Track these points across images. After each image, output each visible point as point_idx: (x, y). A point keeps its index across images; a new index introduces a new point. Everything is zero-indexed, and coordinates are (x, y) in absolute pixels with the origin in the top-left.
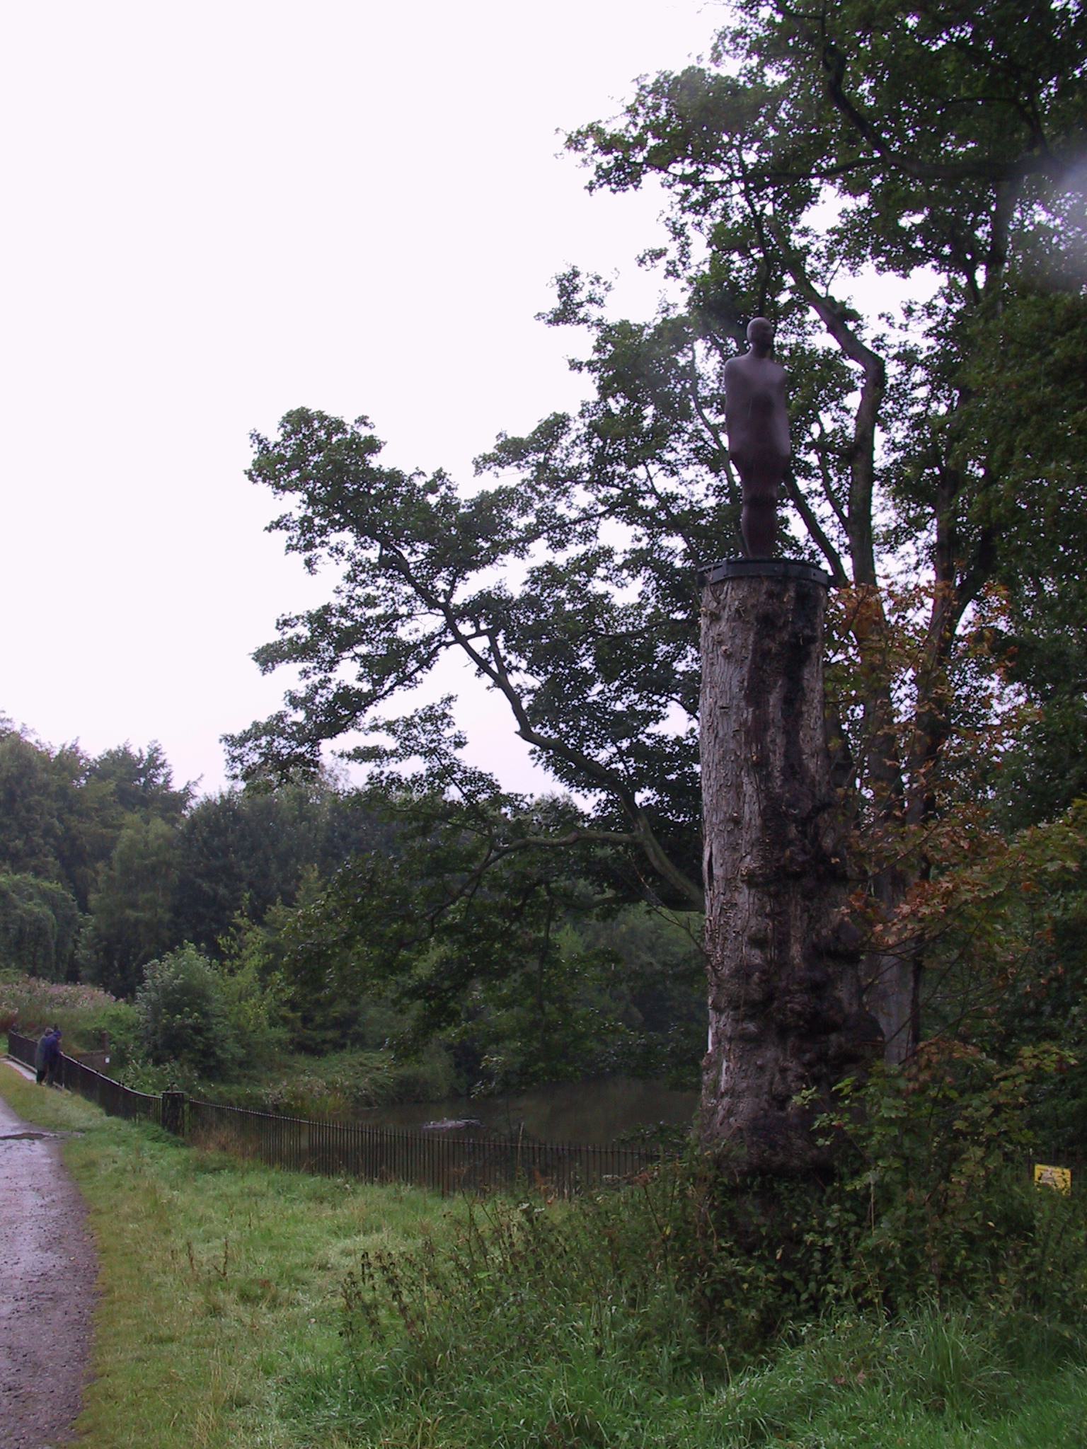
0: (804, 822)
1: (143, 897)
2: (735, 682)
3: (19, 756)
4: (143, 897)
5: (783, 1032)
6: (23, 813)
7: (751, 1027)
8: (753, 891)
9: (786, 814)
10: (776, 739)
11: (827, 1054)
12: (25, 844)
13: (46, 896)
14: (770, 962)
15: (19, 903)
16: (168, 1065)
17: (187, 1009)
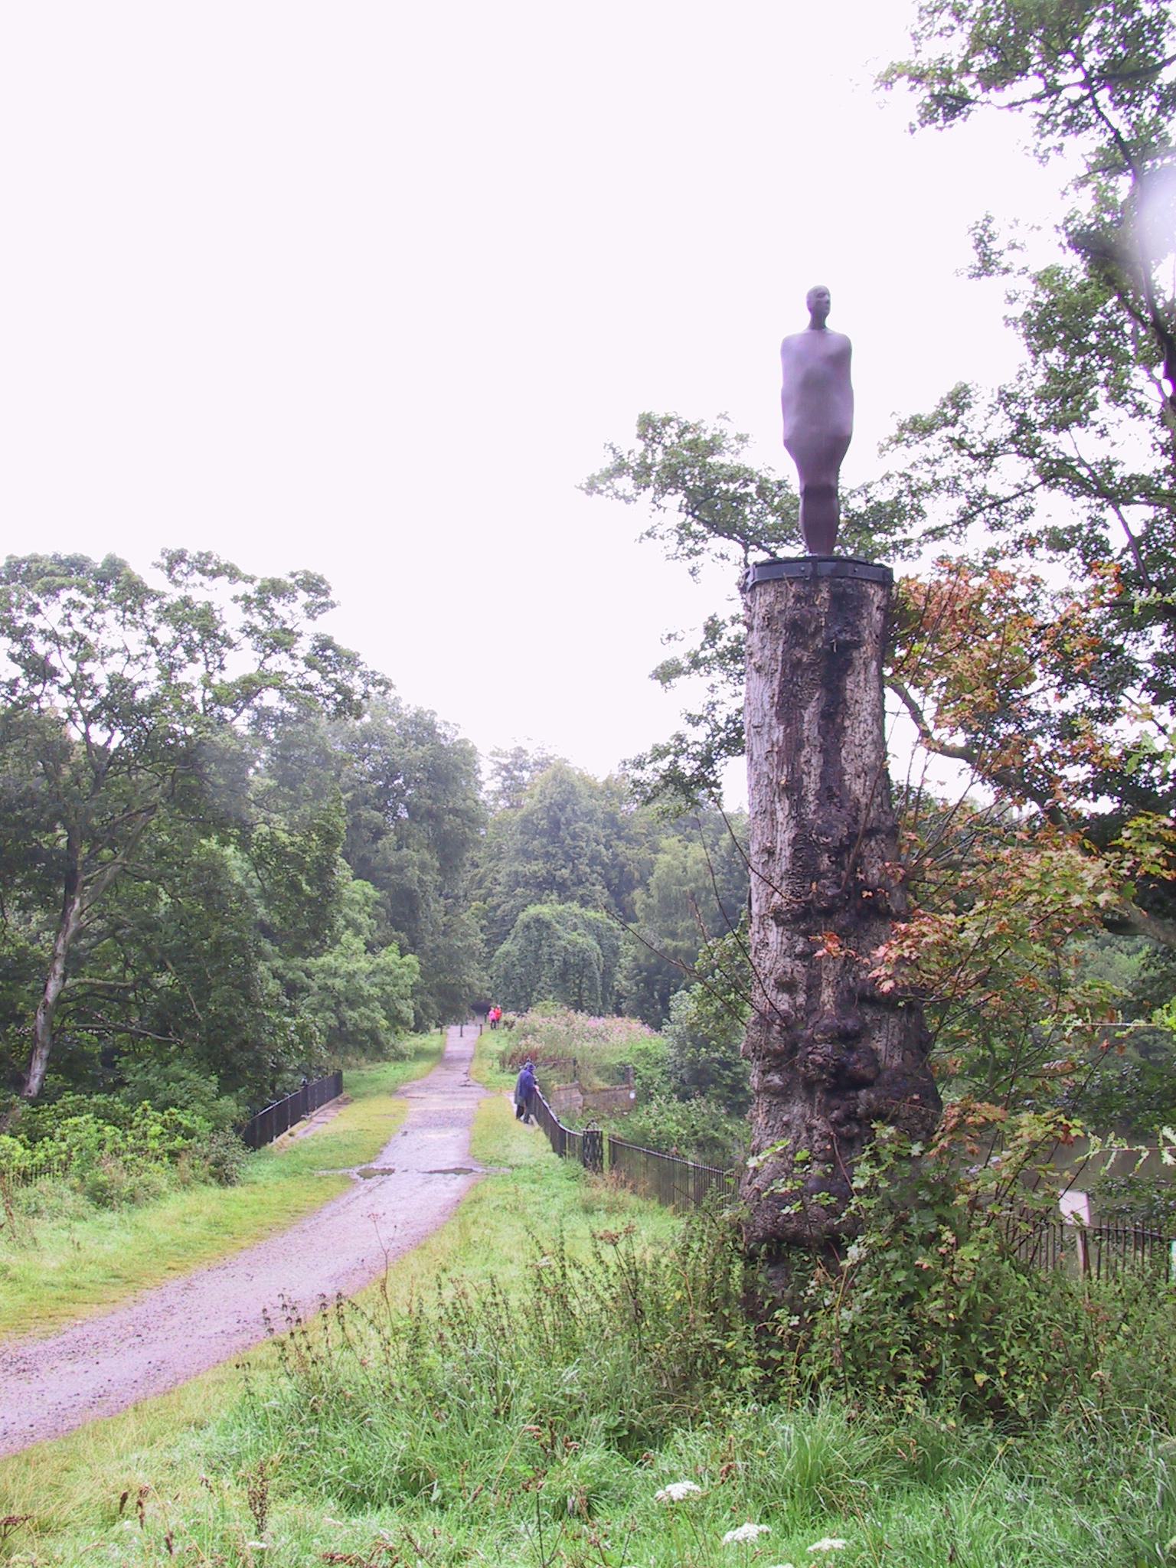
0: (839, 852)
1: (682, 925)
2: (766, 698)
3: (562, 782)
4: (682, 925)
5: (809, 1086)
6: (568, 841)
7: (776, 1079)
8: (781, 929)
9: (817, 844)
10: (812, 760)
11: (856, 1112)
12: (572, 872)
13: (590, 926)
14: (797, 1008)
15: (562, 933)
16: (693, 1100)
17: (713, 1042)
